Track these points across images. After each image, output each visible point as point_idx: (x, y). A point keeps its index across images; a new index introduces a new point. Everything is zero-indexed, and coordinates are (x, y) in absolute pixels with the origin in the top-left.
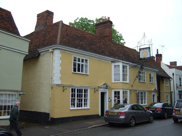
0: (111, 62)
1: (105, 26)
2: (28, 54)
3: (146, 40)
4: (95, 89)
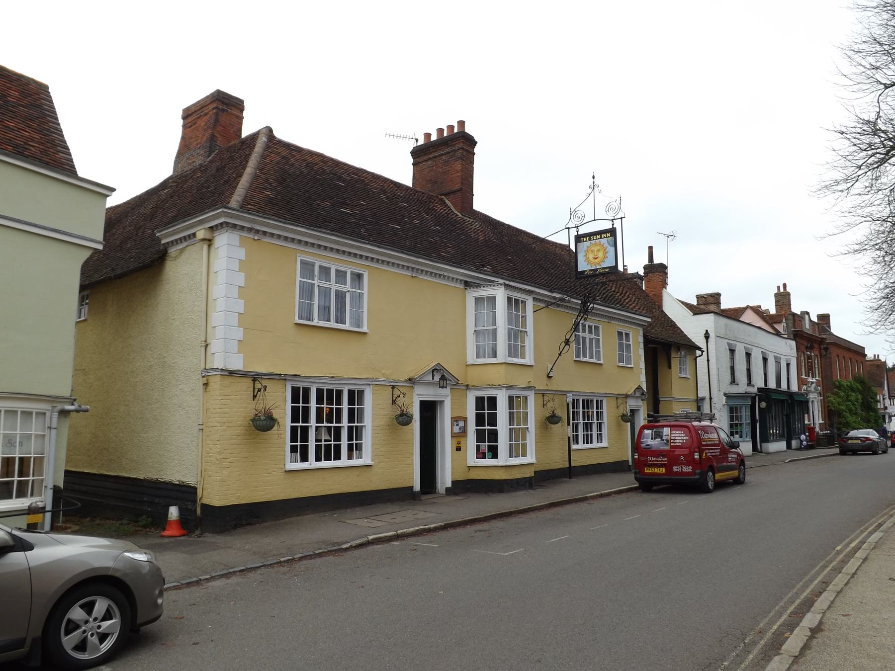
0: (462, 286)
1: (448, 153)
2: (100, 247)
3: (602, 201)
4: (393, 387)
